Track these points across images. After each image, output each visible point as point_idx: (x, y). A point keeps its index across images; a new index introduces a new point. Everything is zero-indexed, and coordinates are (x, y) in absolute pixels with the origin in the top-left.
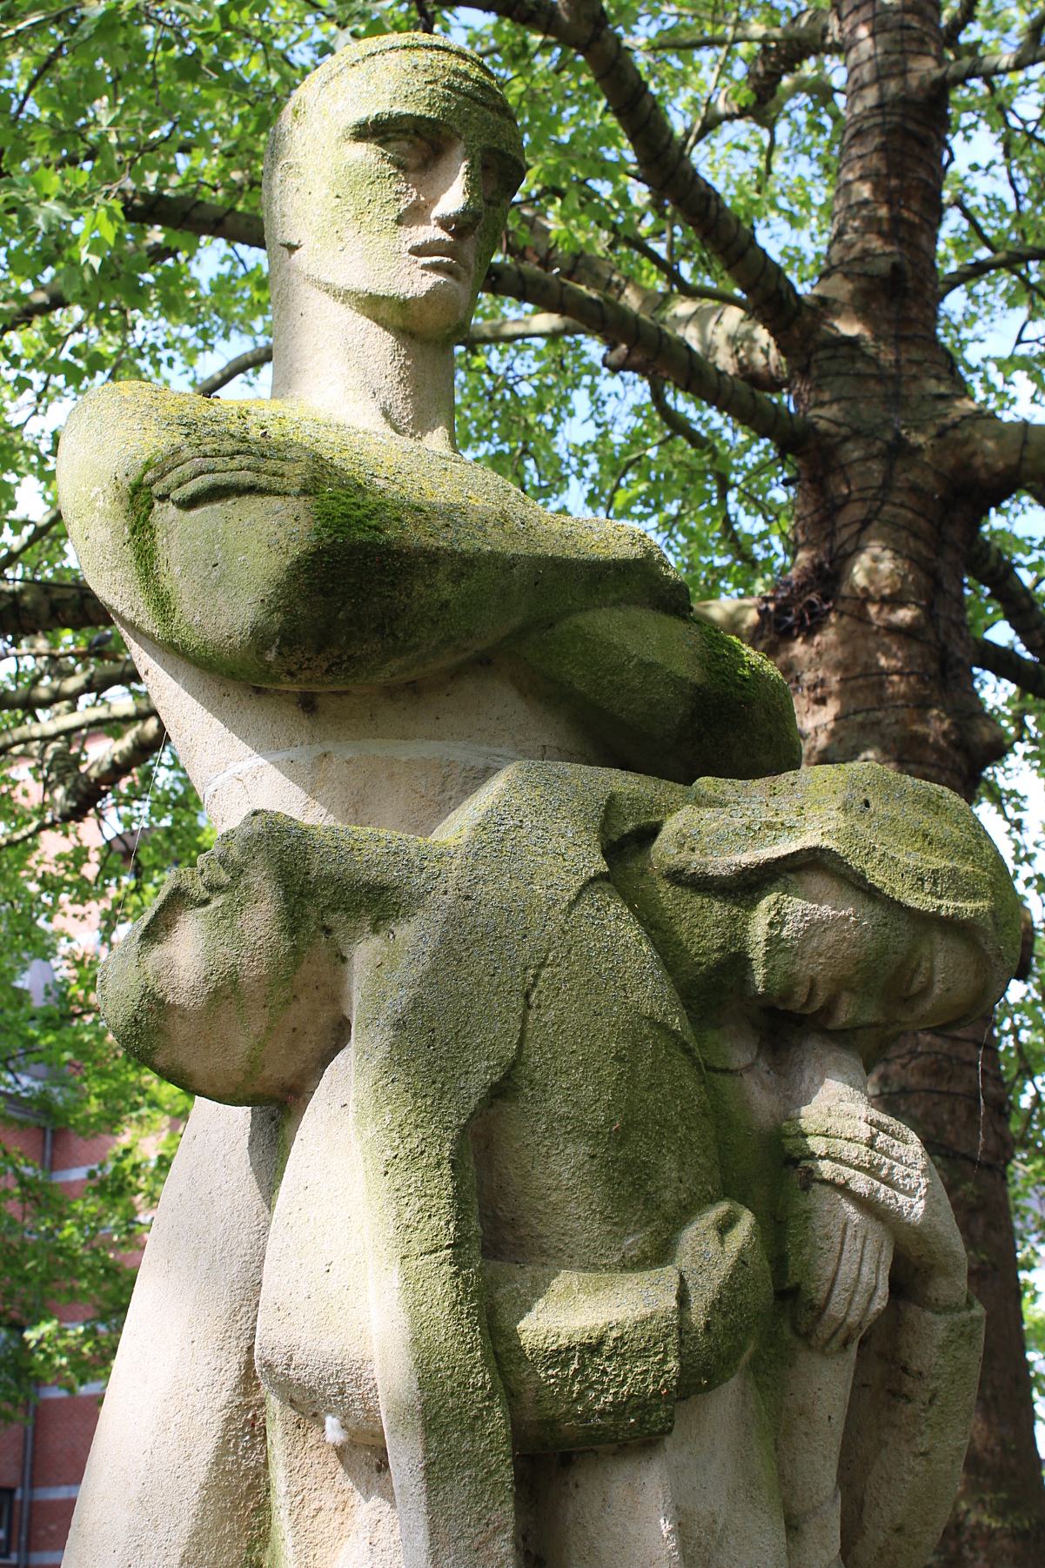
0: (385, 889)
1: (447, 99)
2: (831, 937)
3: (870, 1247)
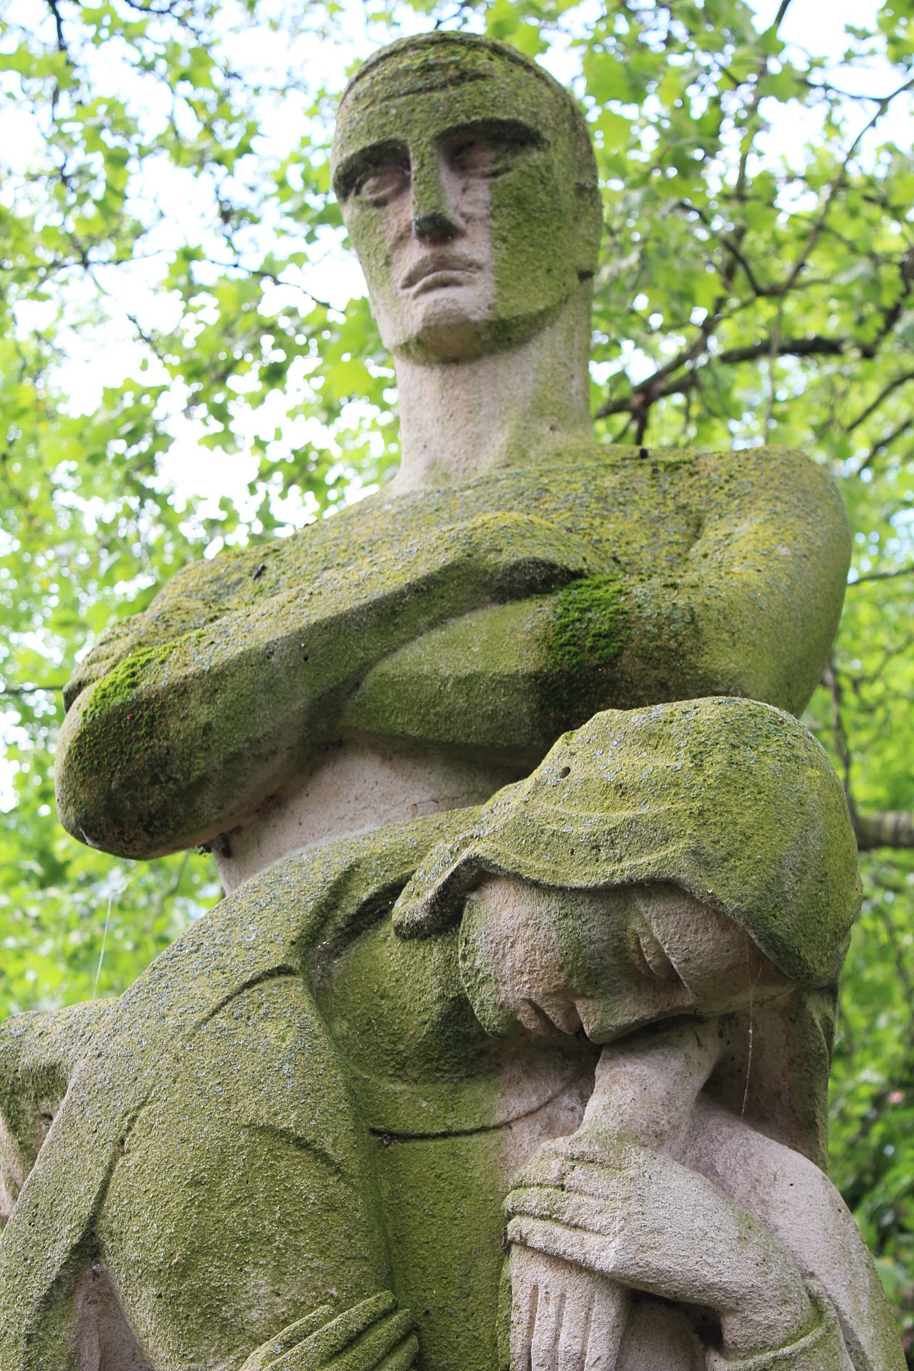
0: (54, 1067)
3: (569, 1307)
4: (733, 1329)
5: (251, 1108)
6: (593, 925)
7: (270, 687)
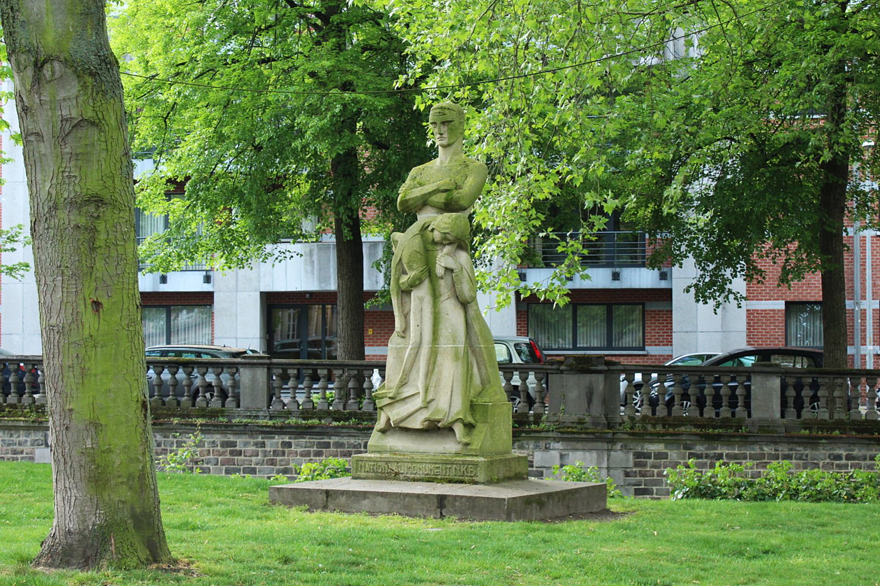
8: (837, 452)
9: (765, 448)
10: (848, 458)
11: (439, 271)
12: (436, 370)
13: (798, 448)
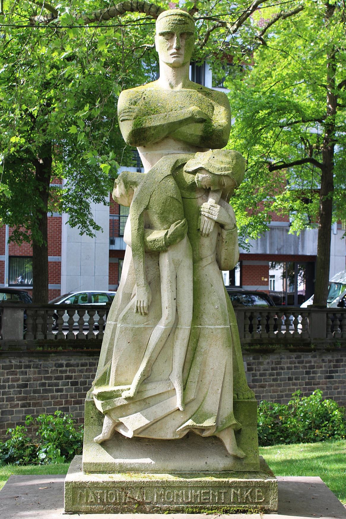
1: (172, 26)
2: (206, 179)
4: (226, 227)
5: (169, 194)
6: (217, 179)
7: (163, 130)
8: (60, 362)
9: (13, 361)
10: (68, 365)
11: (206, 226)
12: (199, 359)
13: (35, 360)
